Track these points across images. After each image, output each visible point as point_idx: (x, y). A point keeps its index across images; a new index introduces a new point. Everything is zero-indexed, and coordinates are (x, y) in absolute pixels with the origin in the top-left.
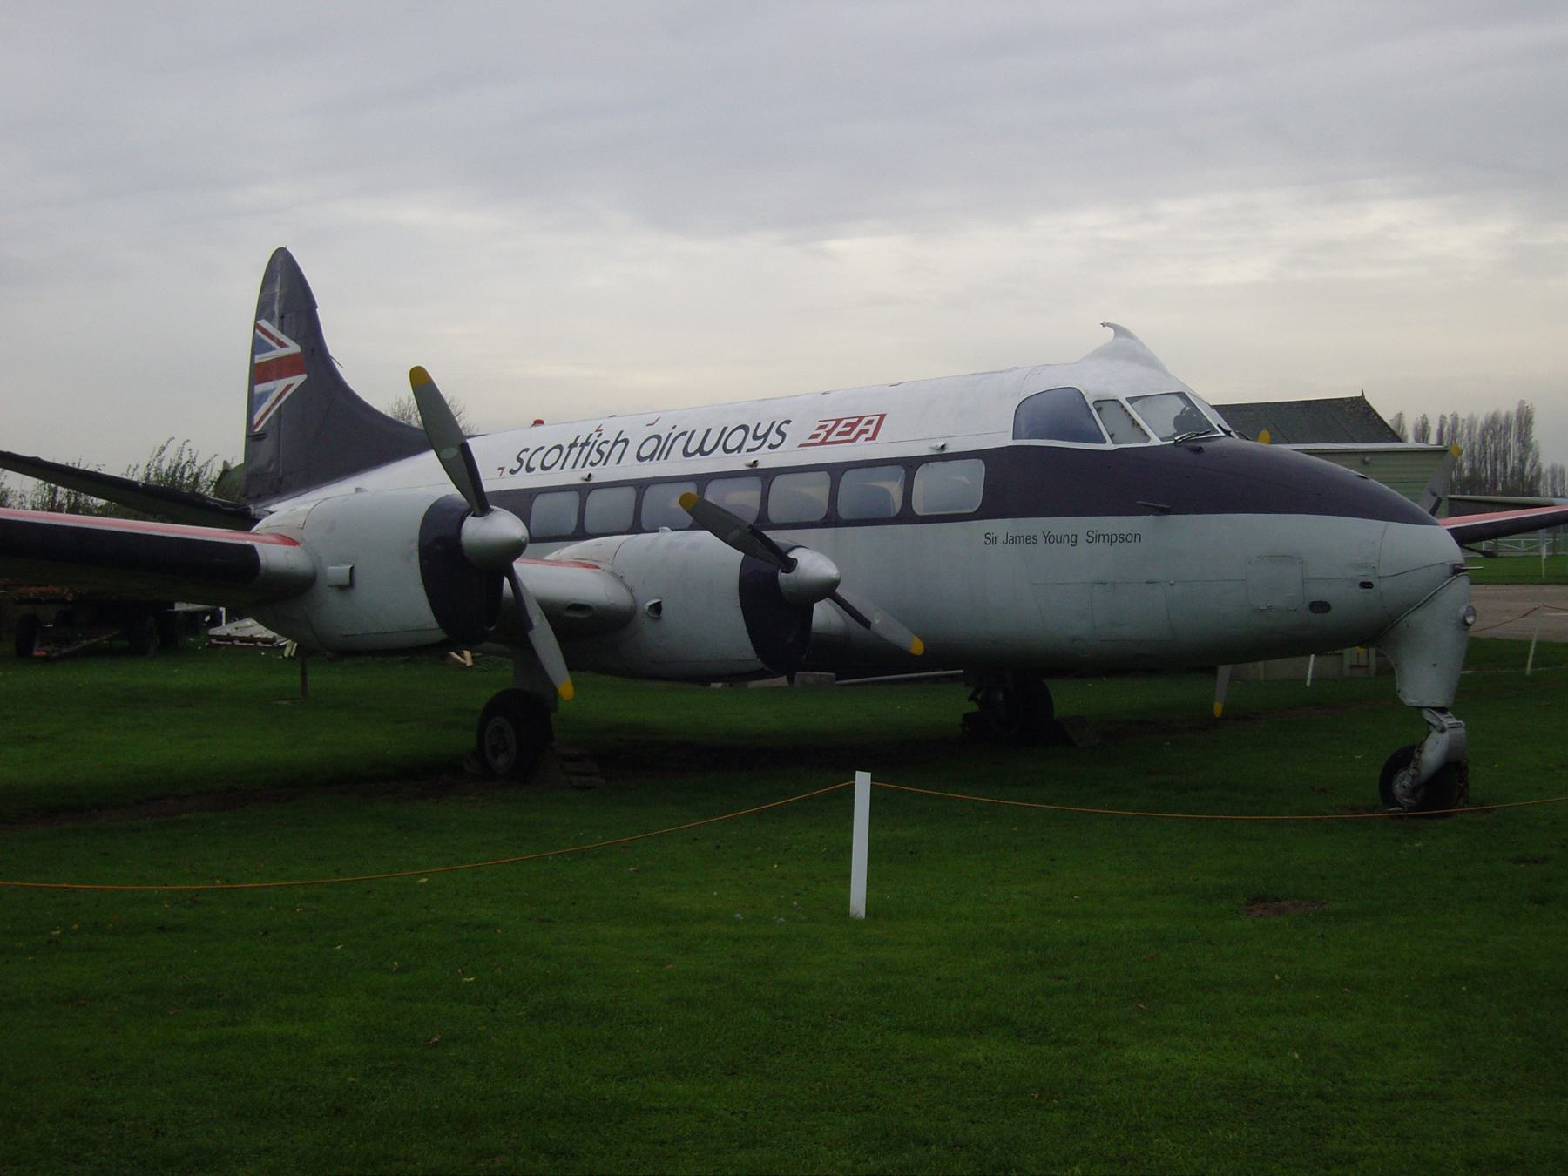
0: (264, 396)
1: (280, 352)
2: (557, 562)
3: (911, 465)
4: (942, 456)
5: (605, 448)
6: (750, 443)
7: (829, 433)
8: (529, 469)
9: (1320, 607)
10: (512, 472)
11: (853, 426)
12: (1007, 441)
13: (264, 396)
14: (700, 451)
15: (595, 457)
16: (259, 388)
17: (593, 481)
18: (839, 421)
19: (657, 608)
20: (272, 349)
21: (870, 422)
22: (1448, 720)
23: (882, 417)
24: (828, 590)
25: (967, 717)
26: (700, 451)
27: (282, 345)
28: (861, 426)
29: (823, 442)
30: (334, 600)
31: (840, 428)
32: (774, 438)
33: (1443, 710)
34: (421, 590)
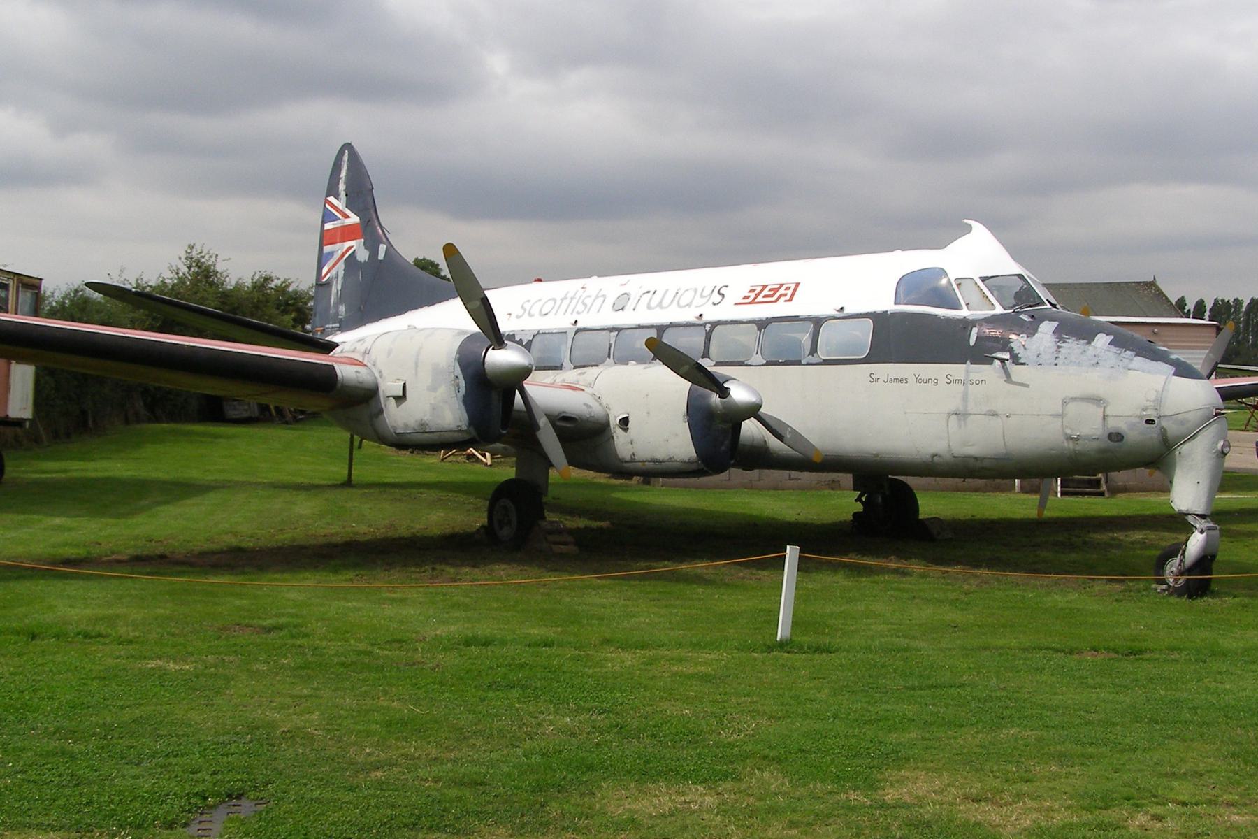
0: (331, 254)
1: (348, 222)
2: (553, 385)
3: (818, 322)
4: (842, 316)
5: (589, 301)
6: (698, 301)
7: (757, 296)
8: (530, 315)
9: (1116, 437)
10: (518, 317)
11: (776, 290)
12: (885, 302)
13: (331, 254)
14: (660, 305)
15: (580, 307)
16: (327, 249)
17: (847, 311)
18: (765, 287)
19: (625, 422)
20: (337, 219)
21: (788, 288)
22: (1200, 524)
23: (798, 284)
24: (753, 411)
25: (856, 515)
26: (660, 305)
27: (347, 217)
28: (782, 291)
29: (752, 302)
30: (618, 435)
31: (766, 292)
32: (717, 298)
33: (1203, 516)
34: (685, 427)
